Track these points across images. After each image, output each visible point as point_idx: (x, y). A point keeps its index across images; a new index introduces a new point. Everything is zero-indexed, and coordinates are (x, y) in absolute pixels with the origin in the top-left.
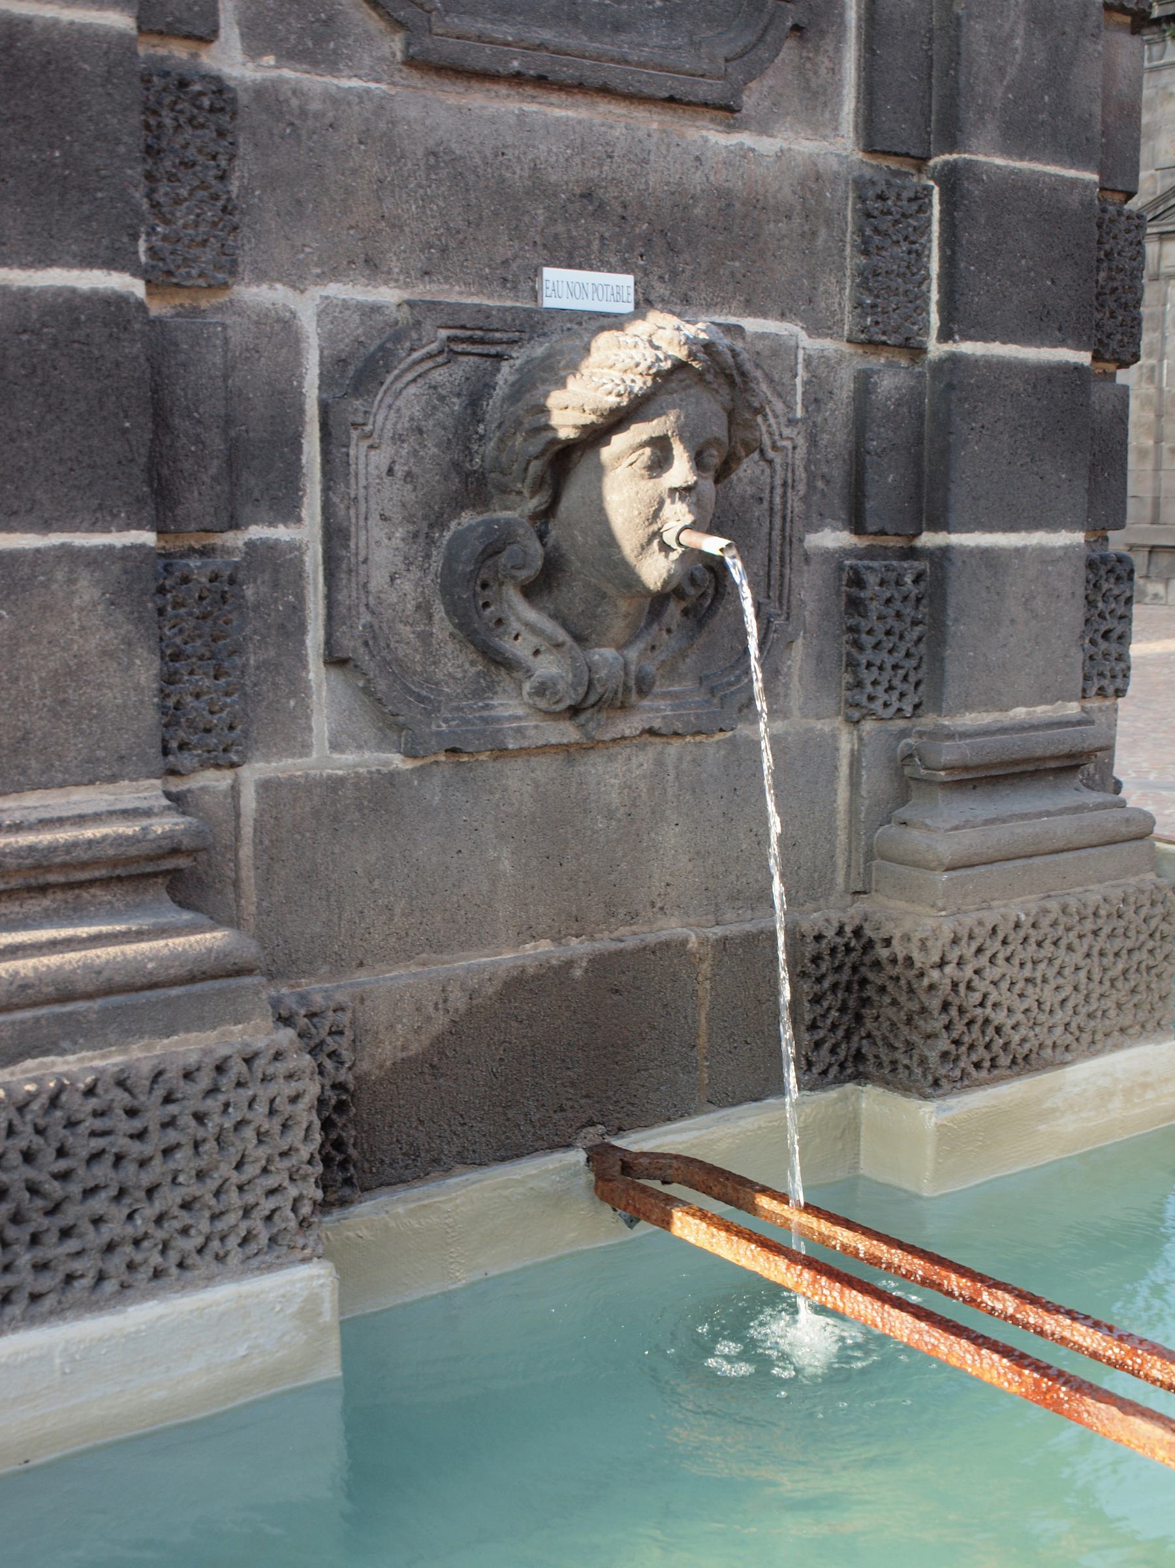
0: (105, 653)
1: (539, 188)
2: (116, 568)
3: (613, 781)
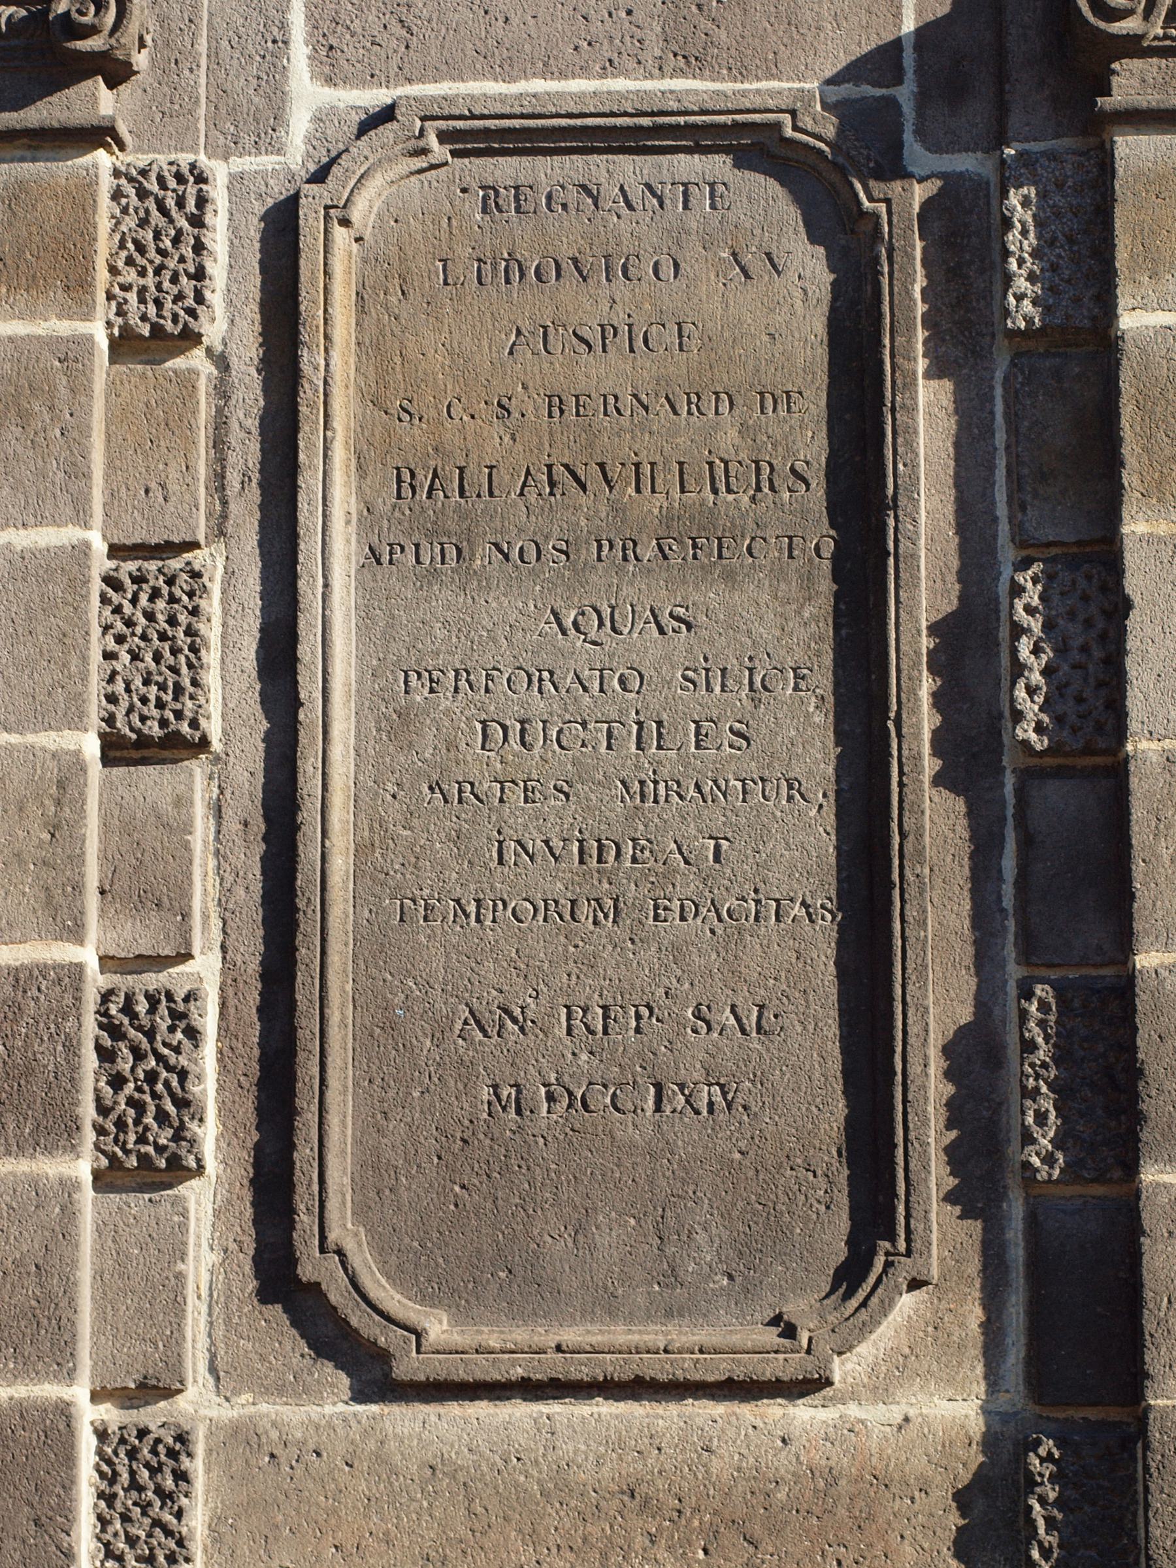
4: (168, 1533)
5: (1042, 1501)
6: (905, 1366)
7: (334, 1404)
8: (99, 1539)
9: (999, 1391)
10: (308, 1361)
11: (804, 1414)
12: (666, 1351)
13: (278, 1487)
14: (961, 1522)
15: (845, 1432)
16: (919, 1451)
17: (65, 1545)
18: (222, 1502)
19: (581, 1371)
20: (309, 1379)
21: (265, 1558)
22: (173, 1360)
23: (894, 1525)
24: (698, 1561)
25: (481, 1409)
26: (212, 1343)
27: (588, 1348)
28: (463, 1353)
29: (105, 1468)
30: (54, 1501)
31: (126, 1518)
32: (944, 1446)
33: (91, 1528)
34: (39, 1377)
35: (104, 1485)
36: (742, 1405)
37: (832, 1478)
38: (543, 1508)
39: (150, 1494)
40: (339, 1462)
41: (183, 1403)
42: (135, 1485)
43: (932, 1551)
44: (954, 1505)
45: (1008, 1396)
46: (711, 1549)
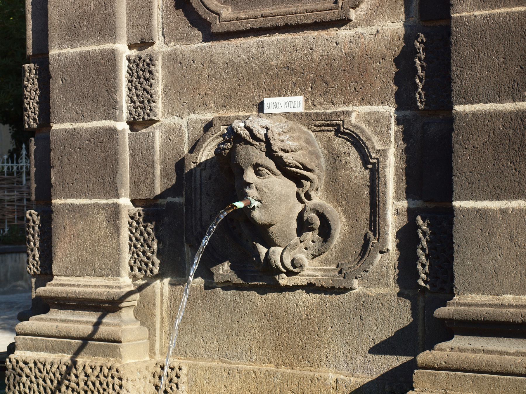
0: (106, 236)
1: (266, 67)
2: (109, 210)
3: (301, 303)
4: (148, 93)
5: (420, 59)
6: (377, 10)
7: (198, 43)
8: (129, 96)
9: (409, 17)
10: (190, 29)
11: (344, 33)
12: (295, 13)
13: (182, 75)
14: (397, 70)
15: (357, 38)
16: (382, 44)
19: (269, 24)
20: (190, 35)
21: (179, 100)
22: (149, 32)
23: (374, 73)
24: (309, 92)
25: (241, 41)
26: (163, 25)
27: (271, 15)
28: (233, 21)
29: (130, 71)
30: (111, 84)
31: (136, 89)
32: (390, 41)
34: (106, 41)
35: (130, 78)
36: (323, 31)
37: (352, 55)
39: (142, 79)
40: (200, 64)
41: (155, 47)
42: (139, 77)
44: (394, 64)
45: (413, 19)
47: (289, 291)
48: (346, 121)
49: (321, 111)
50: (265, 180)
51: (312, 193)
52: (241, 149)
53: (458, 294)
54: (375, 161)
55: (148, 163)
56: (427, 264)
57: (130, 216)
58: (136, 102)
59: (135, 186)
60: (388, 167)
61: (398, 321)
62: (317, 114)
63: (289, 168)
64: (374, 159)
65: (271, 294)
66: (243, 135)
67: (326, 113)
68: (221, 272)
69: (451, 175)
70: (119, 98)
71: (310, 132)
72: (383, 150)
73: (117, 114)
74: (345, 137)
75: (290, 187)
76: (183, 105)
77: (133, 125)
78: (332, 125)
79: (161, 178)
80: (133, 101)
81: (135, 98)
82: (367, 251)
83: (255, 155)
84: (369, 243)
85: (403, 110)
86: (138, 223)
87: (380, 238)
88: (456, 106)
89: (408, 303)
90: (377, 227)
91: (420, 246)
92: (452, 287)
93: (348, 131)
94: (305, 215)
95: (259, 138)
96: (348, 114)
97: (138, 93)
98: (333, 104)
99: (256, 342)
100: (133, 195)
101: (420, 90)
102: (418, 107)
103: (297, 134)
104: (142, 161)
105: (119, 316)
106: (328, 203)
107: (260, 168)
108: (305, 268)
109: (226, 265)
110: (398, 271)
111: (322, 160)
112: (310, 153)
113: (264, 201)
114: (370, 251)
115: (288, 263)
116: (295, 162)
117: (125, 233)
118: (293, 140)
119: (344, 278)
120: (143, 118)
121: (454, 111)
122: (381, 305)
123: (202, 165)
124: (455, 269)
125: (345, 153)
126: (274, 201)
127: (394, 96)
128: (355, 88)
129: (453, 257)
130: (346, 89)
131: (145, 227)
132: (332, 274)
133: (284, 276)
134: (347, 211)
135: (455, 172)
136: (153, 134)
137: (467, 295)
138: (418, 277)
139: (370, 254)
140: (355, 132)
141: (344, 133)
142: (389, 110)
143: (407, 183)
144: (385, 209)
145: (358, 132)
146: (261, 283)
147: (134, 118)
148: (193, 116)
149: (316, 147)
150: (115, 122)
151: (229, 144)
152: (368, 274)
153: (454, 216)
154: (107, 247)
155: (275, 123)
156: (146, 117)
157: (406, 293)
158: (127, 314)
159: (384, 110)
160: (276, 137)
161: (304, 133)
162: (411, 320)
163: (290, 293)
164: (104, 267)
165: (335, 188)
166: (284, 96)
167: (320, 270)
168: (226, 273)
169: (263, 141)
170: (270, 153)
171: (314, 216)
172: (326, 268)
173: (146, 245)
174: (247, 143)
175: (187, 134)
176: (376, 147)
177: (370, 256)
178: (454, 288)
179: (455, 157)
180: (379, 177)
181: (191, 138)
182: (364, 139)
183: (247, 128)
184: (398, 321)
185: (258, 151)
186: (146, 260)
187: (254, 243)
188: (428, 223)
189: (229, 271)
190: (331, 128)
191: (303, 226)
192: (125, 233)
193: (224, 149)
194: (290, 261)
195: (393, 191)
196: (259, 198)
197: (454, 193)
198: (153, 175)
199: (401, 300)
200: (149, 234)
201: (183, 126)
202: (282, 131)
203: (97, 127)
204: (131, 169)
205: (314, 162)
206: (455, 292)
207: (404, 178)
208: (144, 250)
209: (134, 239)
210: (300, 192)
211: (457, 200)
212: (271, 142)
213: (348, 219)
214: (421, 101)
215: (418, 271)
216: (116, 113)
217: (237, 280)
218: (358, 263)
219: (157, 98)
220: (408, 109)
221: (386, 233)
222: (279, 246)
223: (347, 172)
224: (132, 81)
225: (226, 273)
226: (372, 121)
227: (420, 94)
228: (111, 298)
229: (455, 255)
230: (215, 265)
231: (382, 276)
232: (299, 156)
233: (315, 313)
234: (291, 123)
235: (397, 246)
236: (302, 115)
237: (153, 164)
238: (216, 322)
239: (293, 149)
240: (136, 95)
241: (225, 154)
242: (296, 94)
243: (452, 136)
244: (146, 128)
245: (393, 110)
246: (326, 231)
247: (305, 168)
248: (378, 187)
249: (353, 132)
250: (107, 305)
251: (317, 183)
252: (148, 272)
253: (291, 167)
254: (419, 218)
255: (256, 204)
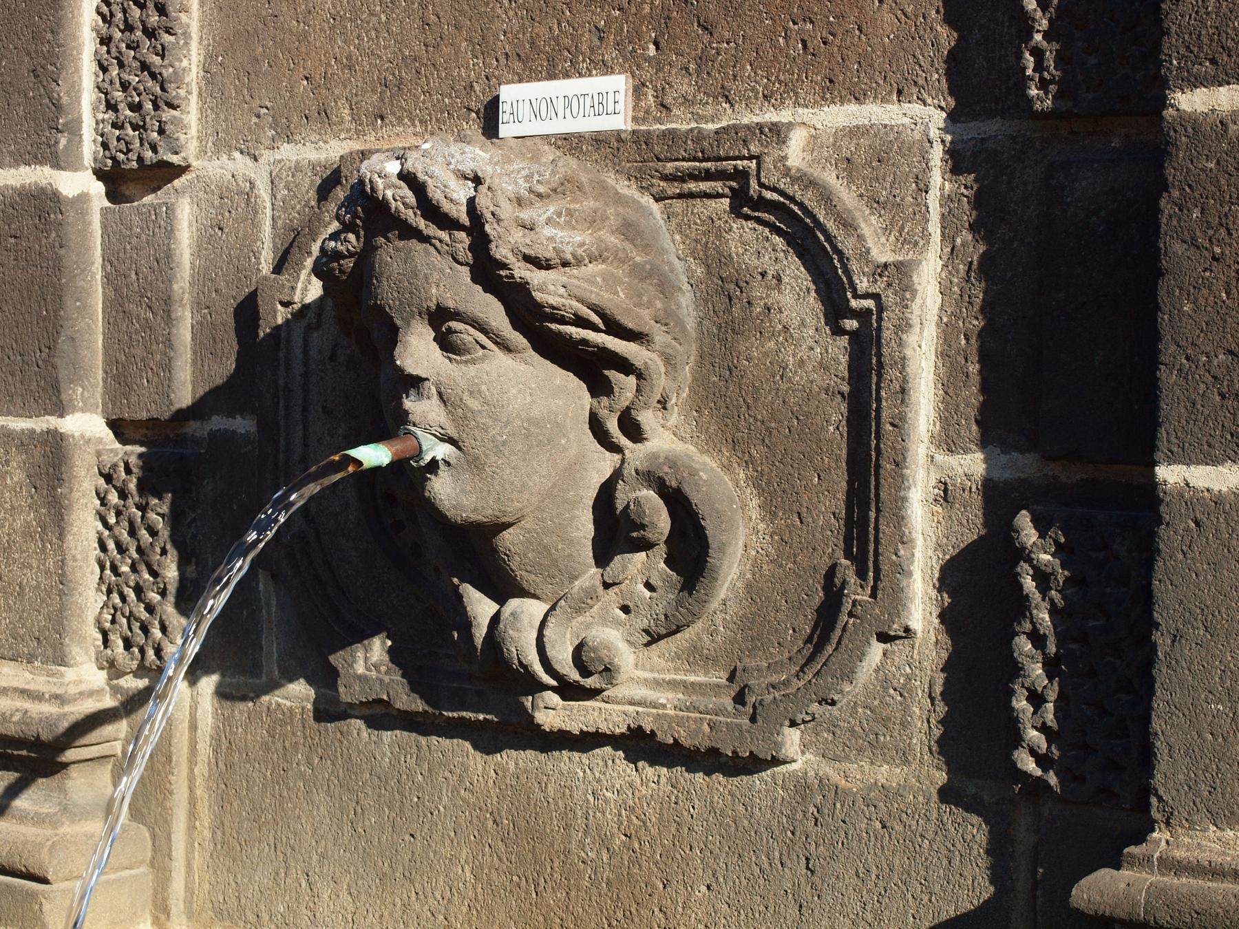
0: (28, 534)
2: (37, 452)
3: (609, 794)
4: (153, 76)
17: (55, 95)
18: (214, 41)
21: (248, 98)
24: (648, 59)
29: (105, 9)
31: (121, 65)
33: (93, 78)
38: (492, 8)
39: (139, 33)
42: (129, 28)
43: (916, 16)
46: (663, 44)
47: (571, 750)
48: (768, 161)
49: (685, 127)
50: (471, 367)
51: (647, 418)
52: (392, 256)
53: (1168, 824)
54: (869, 303)
55: (156, 305)
56: (1052, 695)
57: (101, 474)
58: (121, 106)
59: (120, 379)
60: (917, 329)
61: (937, 889)
62: (672, 135)
63: (554, 326)
64: (866, 296)
65: (513, 753)
66: (393, 205)
67: (700, 131)
68: (360, 669)
69: (1150, 359)
70: (68, 93)
71: (647, 200)
72: (899, 266)
73: (61, 146)
74: (765, 216)
75: (567, 393)
76: (258, 116)
77: (117, 181)
78: (720, 175)
79: (195, 352)
80: (111, 106)
81: (118, 95)
82: (833, 629)
83: (436, 276)
84: (840, 604)
85: (976, 116)
86: (123, 495)
87: (881, 585)
88: (1179, 95)
89: (976, 830)
90: (872, 547)
91: (1027, 626)
92: (1146, 791)
93: (775, 196)
94: (619, 494)
95: (446, 215)
96: (778, 133)
97: (125, 77)
98: (728, 101)
99: (465, 909)
100: (114, 405)
101: (1038, 37)
102: (1030, 101)
103: (589, 204)
104: (140, 296)
105: (62, 790)
106: (702, 452)
107: (454, 325)
108: (622, 677)
109: (378, 648)
110: (942, 709)
111: (686, 301)
112: (636, 270)
113: (467, 443)
114: (844, 629)
115: (562, 657)
116: (575, 304)
117: (85, 527)
118: (569, 226)
119: (753, 719)
120: (140, 159)
121: (1169, 113)
122: (878, 825)
123: (311, 314)
124: (1157, 724)
125: (763, 274)
126: (504, 443)
127: (942, 67)
128: (804, 42)
129: (1152, 681)
130: (774, 46)
131: (143, 508)
132: (711, 702)
133: (553, 698)
134: (769, 483)
135: (1168, 350)
136: (171, 209)
137: (1205, 830)
138: (1016, 739)
139: (845, 641)
140: (798, 197)
141: (761, 204)
142: (924, 118)
143: (985, 388)
144: (900, 482)
145: (809, 198)
146: (481, 717)
147: (113, 158)
148: (288, 152)
149: (663, 251)
150: (55, 173)
151: (352, 237)
152: (835, 711)
153: (1158, 520)
154: (30, 567)
155: (510, 161)
156: (148, 154)
157: (972, 790)
158: (85, 783)
159: (906, 120)
160: (507, 210)
161: (619, 200)
162: (987, 891)
163: (576, 755)
164: (22, 631)
165: (728, 402)
166: (567, 76)
167: (673, 685)
168: (374, 674)
169: (461, 227)
170: (487, 271)
171: (646, 498)
172: (692, 678)
173: (143, 568)
174: (410, 232)
175: (268, 212)
176: (875, 252)
177: (842, 649)
178: (1154, 800)
179: (1170, 293)
180: (880, 365)
181: (280, 223)
182: (830, 225)
183: (407, 177)
184: (937, 889)
185: (445, 263)
186: (144, 615)
187: (455, 580)
188: (1056, 542)
189: (383, 668)
190: (718, 186)
191: (615, 532)
192: (85, 527)
193: (337, 255)
194: (570, 649)
195: (933, 415)
196: (452, 432)
197: (1162, 433)
198: (169, 343)
199: (952, 815)
200: (153, 533)
201: (258, 183)
202: (531, 191)
203: (6, 187)
204: (108, 322)
205: (650, 305)
206: (1155, 814)
207: (974, 368)
208: (137, 584)
209: (111, 545)
210: (603, 413)
211: (1172, 460)
212: (487, 228)
213: (770, 512)
214: (1042, 79)
215: (1016, 721)
216: (57, 143)
217: (407, 701)
218: (802, 670)
219: (182, 92)
220: (991, 114)
221: (902, 570)
222: (535, 596)
223: (772, 344)
224: (110, 38)
225: (374, 674)
226: (860, 159)
227: (1038, 53)
228: (30, 733)
229: (1162, 673)
230: (343, 647)
231: (885, 721)
232: (591, 281)
233: (654, 832)
234: (570, 164)
235: (942, 616)
236: (619, 140)
237: (166, 305)
238: (347, 828)
239: (569, 257)
240: (121, 83)
241: (341, 271)
242: (606, 69)
243: (1158, 210)
244: (155, 190)
245: (939, 118)
246: (690, 552)
247: (614, 328)
248: (879, 400)
249: (792, 199)
250: (24, 753)
251: (661, 382)
252: (151, 653)
253: (563, 321)
254: (1024, 520)
255: (442, 451)
